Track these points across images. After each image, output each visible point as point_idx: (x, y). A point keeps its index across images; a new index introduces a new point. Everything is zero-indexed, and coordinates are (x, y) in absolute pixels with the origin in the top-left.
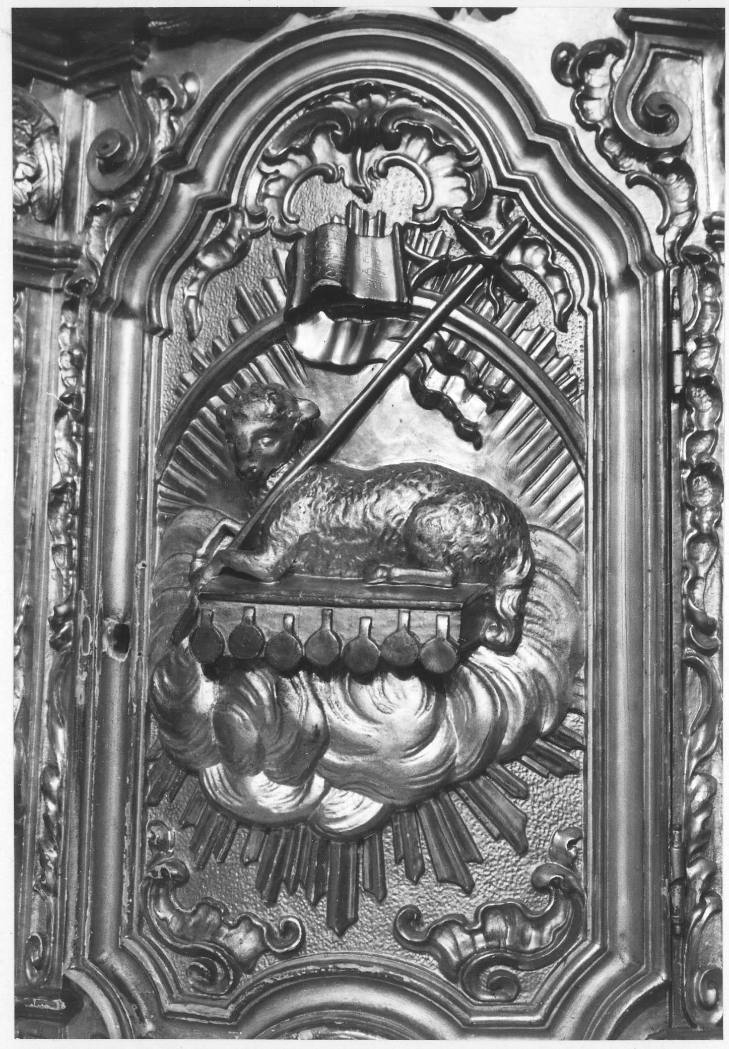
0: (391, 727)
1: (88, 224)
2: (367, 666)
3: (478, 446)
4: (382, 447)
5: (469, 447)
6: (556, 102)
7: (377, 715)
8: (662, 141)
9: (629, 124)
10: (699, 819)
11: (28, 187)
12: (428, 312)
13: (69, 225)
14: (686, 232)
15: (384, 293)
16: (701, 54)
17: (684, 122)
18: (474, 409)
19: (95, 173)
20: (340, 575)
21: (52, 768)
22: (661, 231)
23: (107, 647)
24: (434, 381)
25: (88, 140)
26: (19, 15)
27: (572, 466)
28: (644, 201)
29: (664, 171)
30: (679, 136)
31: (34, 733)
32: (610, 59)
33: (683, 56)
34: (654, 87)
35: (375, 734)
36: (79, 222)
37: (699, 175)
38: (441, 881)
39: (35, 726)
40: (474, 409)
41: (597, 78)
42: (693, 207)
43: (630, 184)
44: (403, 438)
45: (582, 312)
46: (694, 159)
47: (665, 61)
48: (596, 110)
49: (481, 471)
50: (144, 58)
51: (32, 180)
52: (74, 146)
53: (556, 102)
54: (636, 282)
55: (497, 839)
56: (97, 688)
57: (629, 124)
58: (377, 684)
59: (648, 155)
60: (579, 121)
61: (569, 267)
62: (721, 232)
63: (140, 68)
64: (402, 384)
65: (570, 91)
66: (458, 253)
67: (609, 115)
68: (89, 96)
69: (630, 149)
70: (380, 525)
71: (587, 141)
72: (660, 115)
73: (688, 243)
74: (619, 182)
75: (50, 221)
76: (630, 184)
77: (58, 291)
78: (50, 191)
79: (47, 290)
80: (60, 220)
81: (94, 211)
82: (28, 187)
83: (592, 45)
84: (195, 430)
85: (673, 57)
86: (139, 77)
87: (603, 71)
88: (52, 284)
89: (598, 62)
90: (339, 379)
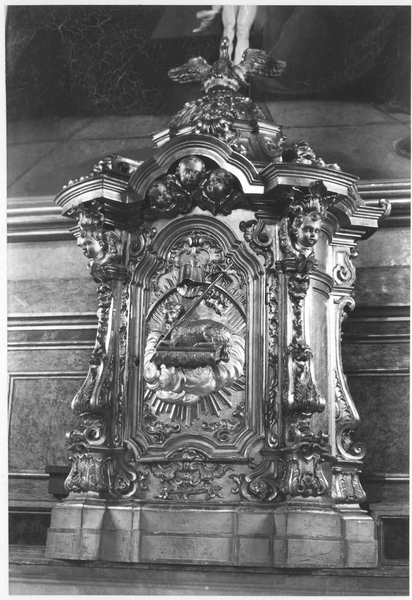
0: (200, 378)
1: (129, 264)
2: (194, 364)
3: (221, 315)
4: (199, 316)
5: (219, 316)
6: (240, 236)
7: (197, 376)
8: (266, 245)
9: (257, 241)
10: (272, 400)
11: (114, 255)
12: (209, 285)
13: (124, 264)
14: (272, 265)
15: (200, 280)
16: (276, 223)
17: (270, 240)
18: (220, 307)
19: (131, 251)
20: (379, 574)
21: (120, 394)
22: (265, 265)
23: (134, 364)
24: (211, 301)
25: (129, 243)
26: (15, 14)
27: (243, 320)
28: (261, 259)
29: (266, 251)
30: (269, 243)
31: (115, 387)
32: (253, 225)
33: (271, 224)
34: (264, 231)
35: (197, 380)
36: (127, 263)
37: (274, 252)
38: (212, 414)
39: (116, 385)
40: (220, 307)
41: (250, 230)
42: (272, 260)
43: (257, 254)
44: (204, 314)
45: (246, 285)
46: (273, 249)
47: (266, 225)
48: (249, 237)
49: (222, 321)
50: (143, 223)
51: (115, 253)
52: (125, 244)
53: (240, 236)
54: (258, 277)
55: (225, 405)
56: (272, 51)
57: (257, 241)
58: (197, 369)
59: (262, 248)
60: (246, 240)
61: (243, 274)
62: (408, 217)
63: (142, 226)
64: (202, 303)
65: (243, 233)
66: (217, 271)
67: (252, 238)
68: (129, 232)
69: (257, 246)
70: (198, 333)
71: (247, 245)
72: (265, 238)
73: (271, 268)
74: (255, 254)
75: (119, 263)
76: (257, 254)
77: (121, 280)
78: (120, 255)
79: (119, 280)
80: (122, 263)
81: (130, 261)
82: (114, 255)
83: (249, 222)
84: (408, 188)
85: (268, 224)
86: (141, 228)
87: (252, 228)
88: (120, 278)
89: (251, 226)
90: (189, 300)
